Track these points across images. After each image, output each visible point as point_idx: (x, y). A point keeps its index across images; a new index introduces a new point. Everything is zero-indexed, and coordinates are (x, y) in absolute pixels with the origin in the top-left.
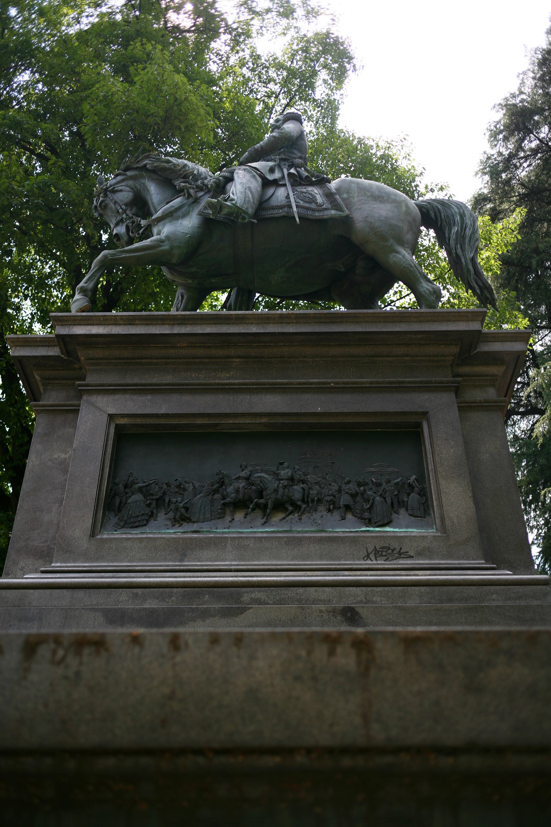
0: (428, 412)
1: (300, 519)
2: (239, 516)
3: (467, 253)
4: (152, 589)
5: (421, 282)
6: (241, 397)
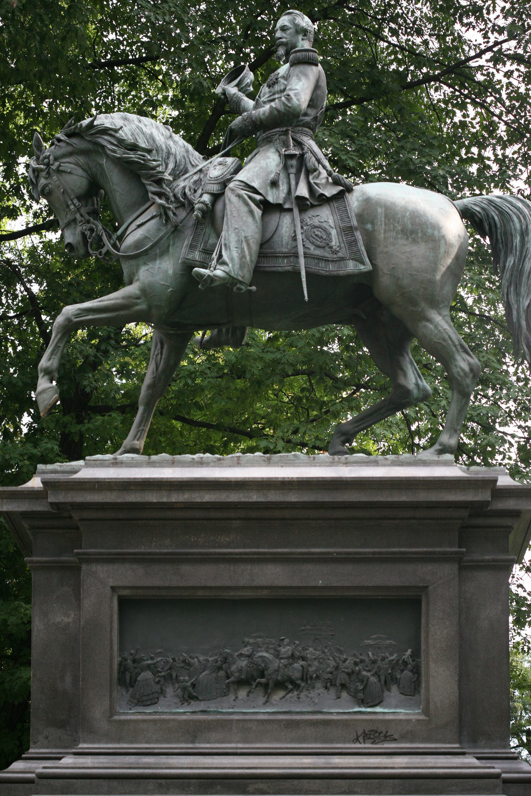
0: (427, 587)
1: (299, 698)
2: (242, 693)
3: (521, 300)
4: (174, 780)
5: (455, 360)
6: (242, 567)
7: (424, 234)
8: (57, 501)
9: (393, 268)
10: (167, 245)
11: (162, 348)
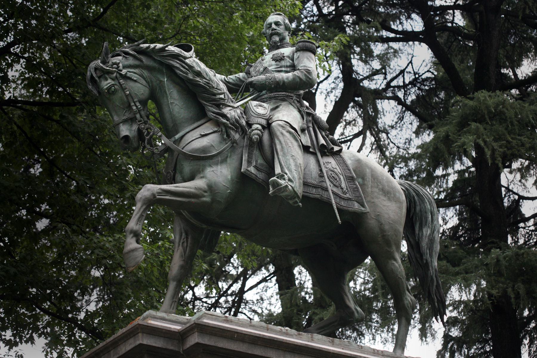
7: (395, 195)
8: (203, 343)
9: (378, 215)
10: (226, 155)
11: (187, 238)
